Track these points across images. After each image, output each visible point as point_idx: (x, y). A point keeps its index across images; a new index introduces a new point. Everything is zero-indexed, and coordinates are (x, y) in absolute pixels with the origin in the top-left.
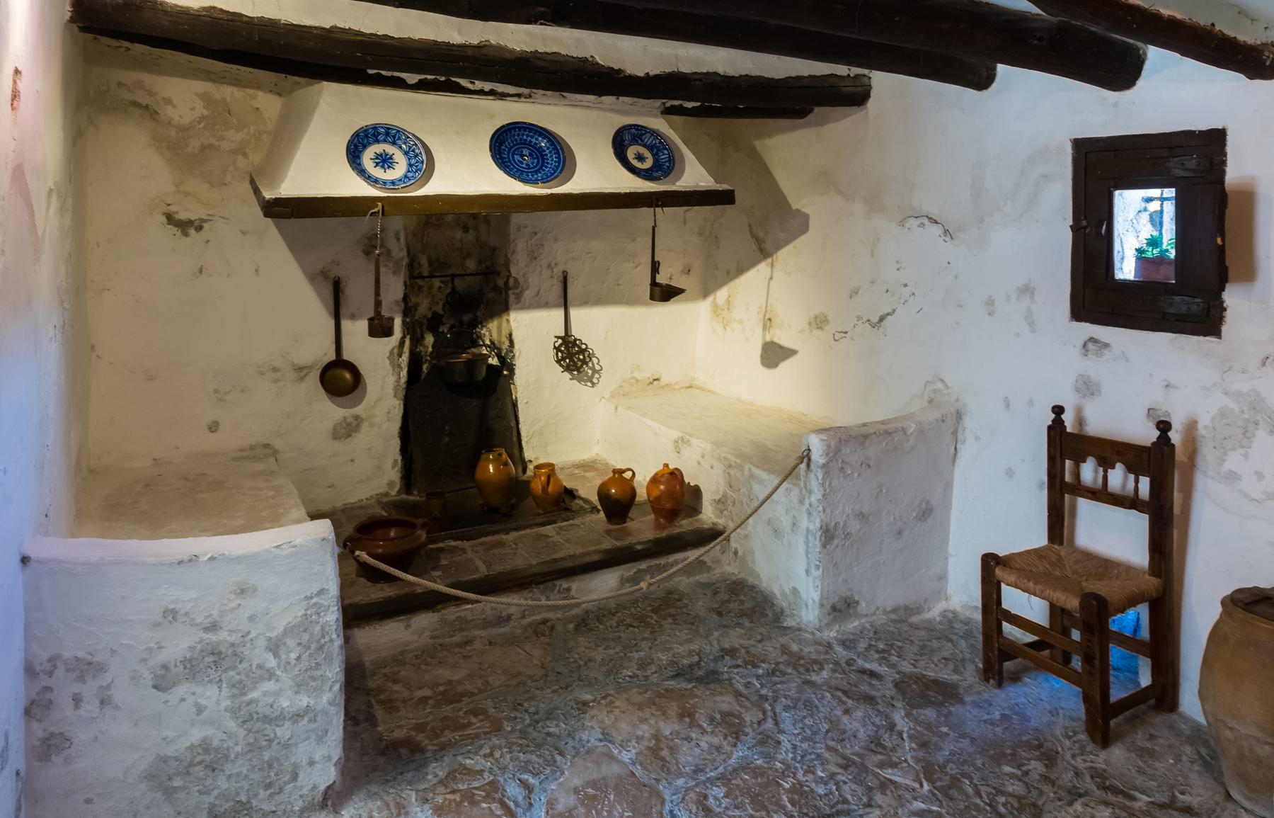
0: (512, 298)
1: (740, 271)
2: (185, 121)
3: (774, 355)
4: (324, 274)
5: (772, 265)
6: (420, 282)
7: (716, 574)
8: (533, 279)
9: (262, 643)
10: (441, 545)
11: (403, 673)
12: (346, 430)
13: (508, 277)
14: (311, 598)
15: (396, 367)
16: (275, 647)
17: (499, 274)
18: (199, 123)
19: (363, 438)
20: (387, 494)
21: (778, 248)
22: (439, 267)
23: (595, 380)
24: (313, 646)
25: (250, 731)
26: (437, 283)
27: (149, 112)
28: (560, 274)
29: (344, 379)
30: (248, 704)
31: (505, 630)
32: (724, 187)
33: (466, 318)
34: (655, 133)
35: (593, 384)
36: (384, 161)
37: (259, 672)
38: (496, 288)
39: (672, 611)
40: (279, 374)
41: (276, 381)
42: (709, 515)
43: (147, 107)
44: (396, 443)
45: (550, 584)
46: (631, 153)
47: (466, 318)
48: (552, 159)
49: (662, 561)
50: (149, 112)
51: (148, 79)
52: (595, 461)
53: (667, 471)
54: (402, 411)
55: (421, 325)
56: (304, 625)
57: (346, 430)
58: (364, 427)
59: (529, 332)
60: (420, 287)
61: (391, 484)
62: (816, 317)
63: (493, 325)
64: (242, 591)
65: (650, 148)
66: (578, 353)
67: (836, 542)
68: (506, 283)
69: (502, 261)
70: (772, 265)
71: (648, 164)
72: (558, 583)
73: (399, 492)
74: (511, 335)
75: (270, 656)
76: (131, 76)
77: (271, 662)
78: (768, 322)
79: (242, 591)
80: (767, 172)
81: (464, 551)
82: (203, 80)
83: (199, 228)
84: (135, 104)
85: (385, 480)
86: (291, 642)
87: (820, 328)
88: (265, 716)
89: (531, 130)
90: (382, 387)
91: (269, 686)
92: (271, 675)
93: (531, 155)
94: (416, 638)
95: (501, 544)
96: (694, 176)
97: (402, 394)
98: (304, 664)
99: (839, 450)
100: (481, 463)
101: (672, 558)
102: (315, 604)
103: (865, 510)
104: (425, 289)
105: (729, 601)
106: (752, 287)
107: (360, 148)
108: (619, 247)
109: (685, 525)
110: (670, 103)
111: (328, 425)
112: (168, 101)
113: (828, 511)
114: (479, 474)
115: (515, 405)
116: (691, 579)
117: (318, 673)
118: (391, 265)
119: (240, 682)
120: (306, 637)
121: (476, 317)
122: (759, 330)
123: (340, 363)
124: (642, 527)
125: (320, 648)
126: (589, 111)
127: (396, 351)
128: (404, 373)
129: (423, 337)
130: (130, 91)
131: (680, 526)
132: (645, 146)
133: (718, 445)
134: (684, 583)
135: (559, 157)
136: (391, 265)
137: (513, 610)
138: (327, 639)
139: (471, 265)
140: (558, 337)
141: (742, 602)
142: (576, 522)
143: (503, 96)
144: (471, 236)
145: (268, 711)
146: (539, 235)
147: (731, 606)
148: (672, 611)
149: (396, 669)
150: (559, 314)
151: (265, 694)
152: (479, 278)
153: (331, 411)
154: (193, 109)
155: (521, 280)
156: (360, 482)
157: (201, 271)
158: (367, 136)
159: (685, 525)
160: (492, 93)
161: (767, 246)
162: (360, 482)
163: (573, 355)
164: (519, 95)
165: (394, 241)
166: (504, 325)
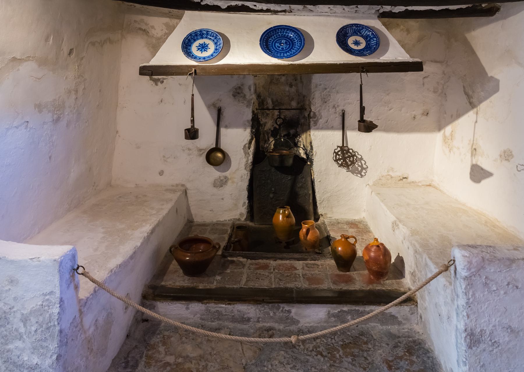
0: (312, 123)
1: (459, 115)
2: (159, 35)
3: (478, 174)
4: (214, 105)
5: (477, 113)
6: (268, 112)
7: (405, 328)
8: (324, 113)
9: (19, 315)
10: (235, 259)
11: (172, 339)
12: (220, 183)
13: (310, 111)
14: (46, 295)
15: (246, 154)
16: (25, 320)
17: (306, 109)
18: (164, 36)
19: (229, 188)
20: (239, 220)
21: (480, 102)
22: (278, 105)
23: (363, 174)
24: (44, 326)
25: (7, 368)
26: (276, 113)
27: (145, 32)
28: (341, 111)
29: (218, 157)
30: (8, 351)
31: (245, 327)
32: (418, 60)
33: (292, 132)
34: (367, 28)
35: (362, 176)
36: (203, 47)
37: (16, 333)
38: (304, 117)
39: (356, 351)
40: (191, 152)
41: (189, 155)
42: (407, 282)
43: (145, 30)
44: (245, 194)
45: (276, 305)
46: (350, 41)
47: (292, 132)
48: (297, 44)
49: (361, 308)
50: (145, 32)
51: (145, 18)
52: (360, 222)
53: (376, 243)
54: (249, 177)
55: (268, 134)
56: (40, 311)
57: (220, 183)
58: (229, 182)
59: (321, 143)
60: (267, 114)
61: (241, 214)
62: (505, 152)
63: (304, 136)
64: (12, 282)
65: (366, 38)
66: (349, 157)
67: (482, 346)
68: (309, 115)
69: (307, 103)
70: (477, 113)
71: (362, 46)
72: (282, 305)
73: (246, 220)
74: (311, 143)
75: (22, 325)
76: (139, 17)
77: (22, 330)
78: (474, 151)
79: (12, 282)
80: (473, 52)
81: (244, 266)
82: (166, 17)
83: (162, 82)
84: (140, 29)
85: (238, 212)
86: (33, 320)
87: (507, 160)
88: (15, 363)
89: (288, 29)
90: (239, 163)
91: (19, 344)
92: (21, 338)
93: (286, 43)
94: (192, 316)
95: (266, 267)
96: (395, 53)
97: (249, 168)
98: (38, 336)
99: (483, 267)
100: (276, 214)
101: (368, 308)
102: (48, 300)
103: (515, 325)
104: (271, 115)
105: (401, 358)
106: (464, 126)
107: (192, 41)
108: (344, 95)
109: (388, 284)
110: (387, 8)
111: (212, 179)
112: (153, 27)
113: (472, 317)
114: (274, 220)
115: (313, 182)
116: (384, 327)
117: (45, 344)
118: (245, 102)
119: (6, 336)
120: (41, 319)
121: (297, 132)
122: (469, 155)
123: (217, 149)
124: (359, 280)
125: (48, 328)
126: (328, 18)
127: (247, 146)
128: (251, 158)
129: (269, 140)
130: (139, 24)
131: (383, 285)
132: (362, 36)
133: (414, 232)
134: (378, 329)
135: (301, 44)
136: (245, 102)
137: (251, 315)
138: (52, 324)
139: (294, 104)
140: (338, 147)
141: (412, 363)
142: (319, 262)
143: (276, 12)
144: (293, 89)
145: (15, 358)
146: (328, 90)
147: (402, 363)
148: (356, 351)
149: (172, 334)
150: (339, 134)
151: (16, 348)
152: (298, 111)
153: (214, 173)
154: (162, 30)
155: (317, 113)
156: (226, 211)
157: (162, 101)
158: (196, 35)
159: (388, 284)
160: (268, 11)
161: (474, 100)
162: (226, 211)
163: (346, 157)
164: (285, 11)
165: (247, 90)
166: (308, 137)
